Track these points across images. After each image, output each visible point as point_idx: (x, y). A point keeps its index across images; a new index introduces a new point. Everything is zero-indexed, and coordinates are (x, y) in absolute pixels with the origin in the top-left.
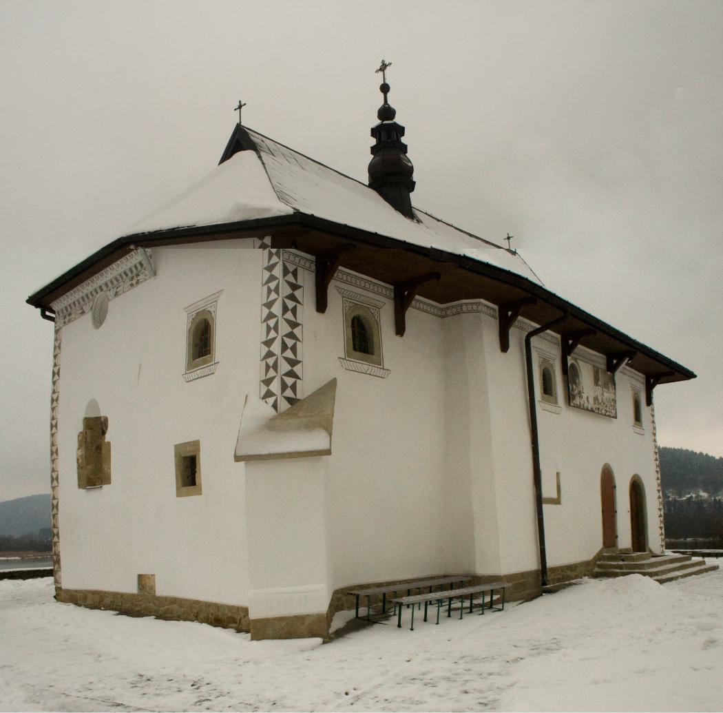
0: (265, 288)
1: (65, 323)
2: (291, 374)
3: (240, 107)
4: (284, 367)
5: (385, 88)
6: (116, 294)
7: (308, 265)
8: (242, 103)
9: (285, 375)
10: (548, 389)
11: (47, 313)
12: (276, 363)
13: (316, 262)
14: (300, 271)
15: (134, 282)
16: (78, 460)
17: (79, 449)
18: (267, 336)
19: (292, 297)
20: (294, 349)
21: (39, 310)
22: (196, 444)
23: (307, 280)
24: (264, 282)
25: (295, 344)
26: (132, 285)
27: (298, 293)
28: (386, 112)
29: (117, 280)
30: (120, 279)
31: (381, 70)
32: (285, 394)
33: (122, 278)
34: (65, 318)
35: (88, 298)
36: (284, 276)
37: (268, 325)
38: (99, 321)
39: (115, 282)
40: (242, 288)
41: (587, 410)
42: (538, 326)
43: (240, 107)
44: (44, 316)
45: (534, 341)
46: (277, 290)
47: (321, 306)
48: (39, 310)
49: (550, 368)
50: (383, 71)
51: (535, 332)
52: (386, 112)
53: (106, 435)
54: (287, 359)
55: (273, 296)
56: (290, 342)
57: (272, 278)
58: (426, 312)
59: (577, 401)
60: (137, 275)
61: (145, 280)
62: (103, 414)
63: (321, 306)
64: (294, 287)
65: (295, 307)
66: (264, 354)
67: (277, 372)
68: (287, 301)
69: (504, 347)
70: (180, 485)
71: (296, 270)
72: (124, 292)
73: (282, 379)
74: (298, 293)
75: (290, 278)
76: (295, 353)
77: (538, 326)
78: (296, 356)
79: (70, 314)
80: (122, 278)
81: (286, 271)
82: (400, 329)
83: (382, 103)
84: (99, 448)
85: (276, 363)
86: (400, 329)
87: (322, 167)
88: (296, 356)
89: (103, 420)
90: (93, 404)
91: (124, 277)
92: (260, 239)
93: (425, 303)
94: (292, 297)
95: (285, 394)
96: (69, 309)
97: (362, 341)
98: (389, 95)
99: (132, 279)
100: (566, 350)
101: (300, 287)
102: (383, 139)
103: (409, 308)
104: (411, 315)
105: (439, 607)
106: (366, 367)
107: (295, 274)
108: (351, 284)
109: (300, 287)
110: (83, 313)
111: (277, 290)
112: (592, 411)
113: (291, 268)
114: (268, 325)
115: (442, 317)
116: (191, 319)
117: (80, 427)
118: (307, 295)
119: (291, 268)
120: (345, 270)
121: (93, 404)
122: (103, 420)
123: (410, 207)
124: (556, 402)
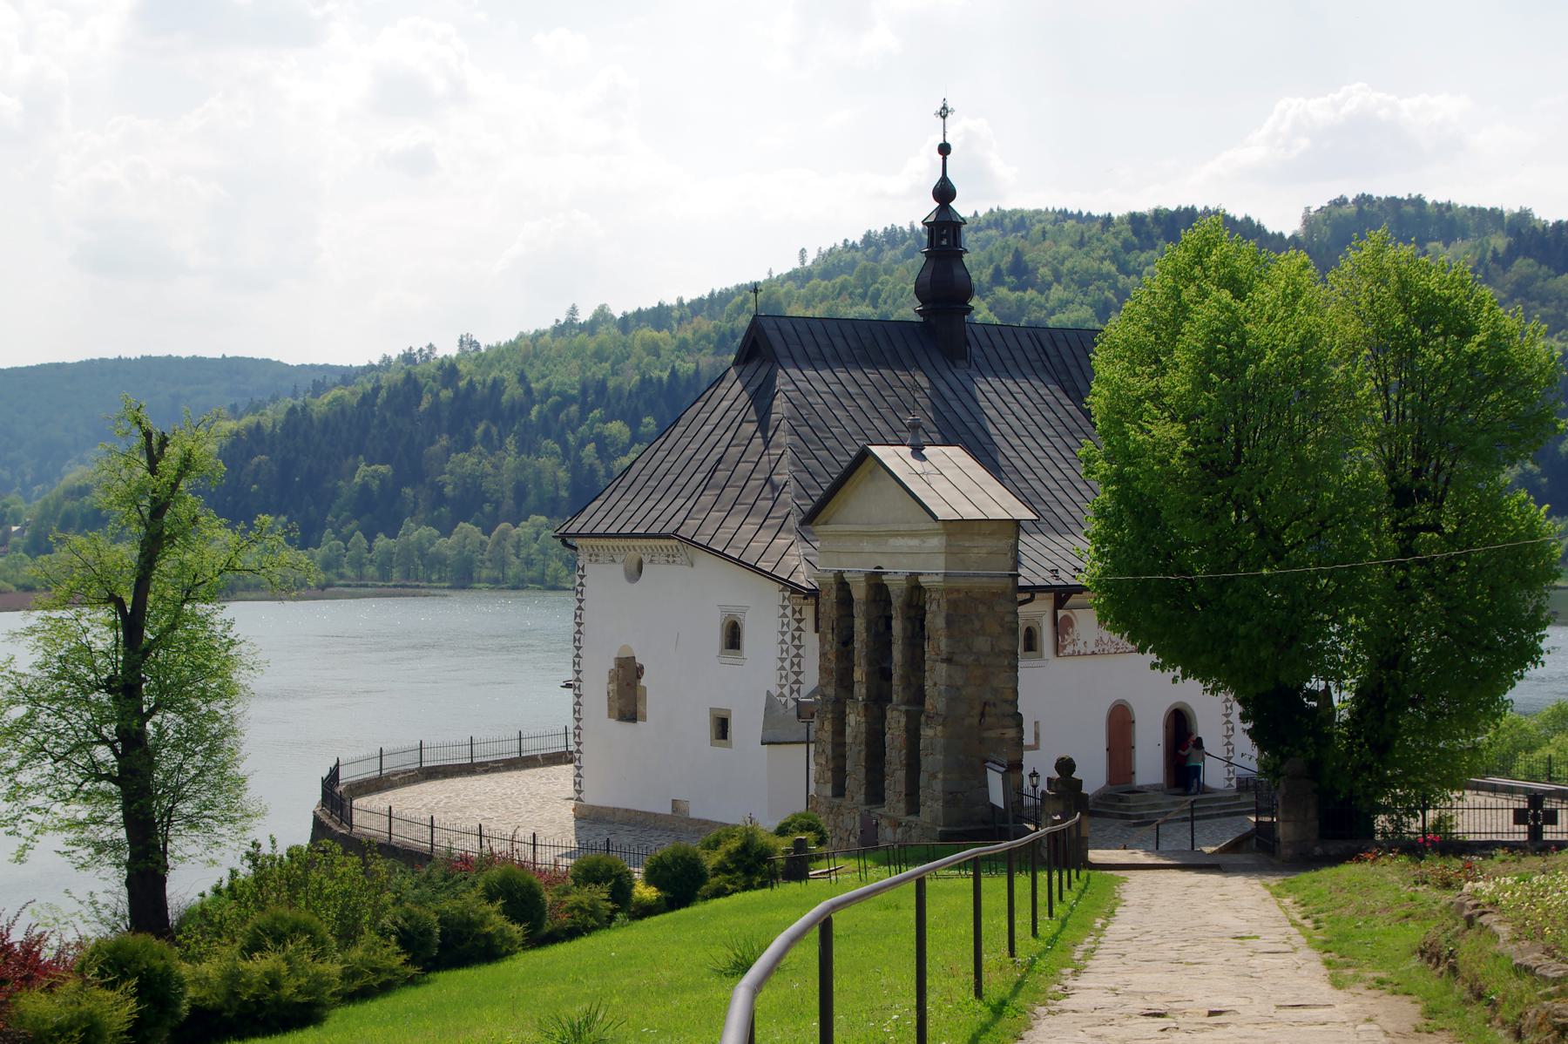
40: (1061, 613)
57: (784, 615)
59: (1069, 650)
112: (1093, 653)
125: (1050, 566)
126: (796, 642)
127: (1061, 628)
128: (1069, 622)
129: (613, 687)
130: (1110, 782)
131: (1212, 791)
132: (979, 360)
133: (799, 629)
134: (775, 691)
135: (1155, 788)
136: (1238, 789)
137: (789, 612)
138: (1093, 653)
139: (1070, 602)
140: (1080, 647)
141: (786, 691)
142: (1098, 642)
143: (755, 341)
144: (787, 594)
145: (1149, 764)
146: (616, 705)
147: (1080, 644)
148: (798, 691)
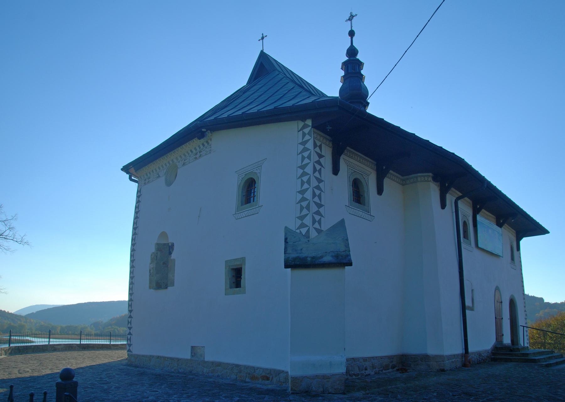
0: (300, 156)
1: (145, 183)
2: (318, 213)
3: (263, 38)
5: (352, 34)
6: (184, 164)
7: (328, 143)
8: (264, 35)
9: (314, 213)
10: (466, 236)
11: (133, 178)
12: (308, 205)
14: (323, 146)
15: (198, 156)
16: (150, 271)
17: (151, 263)
18: (301, 188)
19: (319, 163)
20: (320, 197)
21: (128, 175)
22: (243, 259)
23: (327, 152)
24: (299, 152)
25: (320, 193)
26: (196, 158)
27: (322, 160)
28: (352, 52)
29: (185, 155)
30: (187, 155)
31: (349, 19)
32: (315, 226)
33: (189, 154)
34: (145, 180)
35: (163, 167)
36: (314, 148)
37: (302, 180)
38: (169, 183)
39: (183, 157)
42: (460, 194)
43: (263, 38)
44: (131, 179)
45: (460, 203)
46: (309, 157)
47: (336, 171)
48: (128, 175)
49: (467, 221)
50: (351, 20)
51: (459, 198)
52: (352, 52)
53: (172, 255)
55: (306, 161)
56: (317, 192)
57: (306, 149)
58: (394, 180)
60: (200, 152)
61: (206, 154)
62: (170, 241)
63: (336, 171)
64: (320, 156)
65: (321, 169)
66: (298, 199)
67: (309, 211)
68: (316, 164)
69: (443, 206)
70: (228, 286)
72: (189, 163)
73: (313, 216)
74: (322, 160)
75: (317, 149)
77: (460, 194)
78: (321, 201)
79: (149, 178)
80: (189, 154)
81: (315, 145)
82: (380, 191)
83: (350, 45)
84: (166, 264)
85: (308, 205)
86: (380, 191)
87: (273, 101)
88: (321, 201)
89: (170, 245)
90: (164, 235)
91: (190, 153)
92: (302, 121)
94: (319, 163)
95: (315, 226)
96: (149, 175)
97: (358, 195)
98: (354, 38)
99: (196, 154)
100: (476, 212)
101: (324, 156)
102: (349, 71)
104: (387, 182)
107: (320, 147)
109: (324, 156)
110: (159, 177)
111: (309, 157)
113: (318, 143)
114: (302, 180)
116: (241, 178)
117: (153, 249)
118: (327, 161)
119: (318, 143)
121: (164, 235)
122: (170, 245)
124: (470, 244)
134: (292, 227)
137: (310, 145)
141: (308, 221)
143: (262, 64)
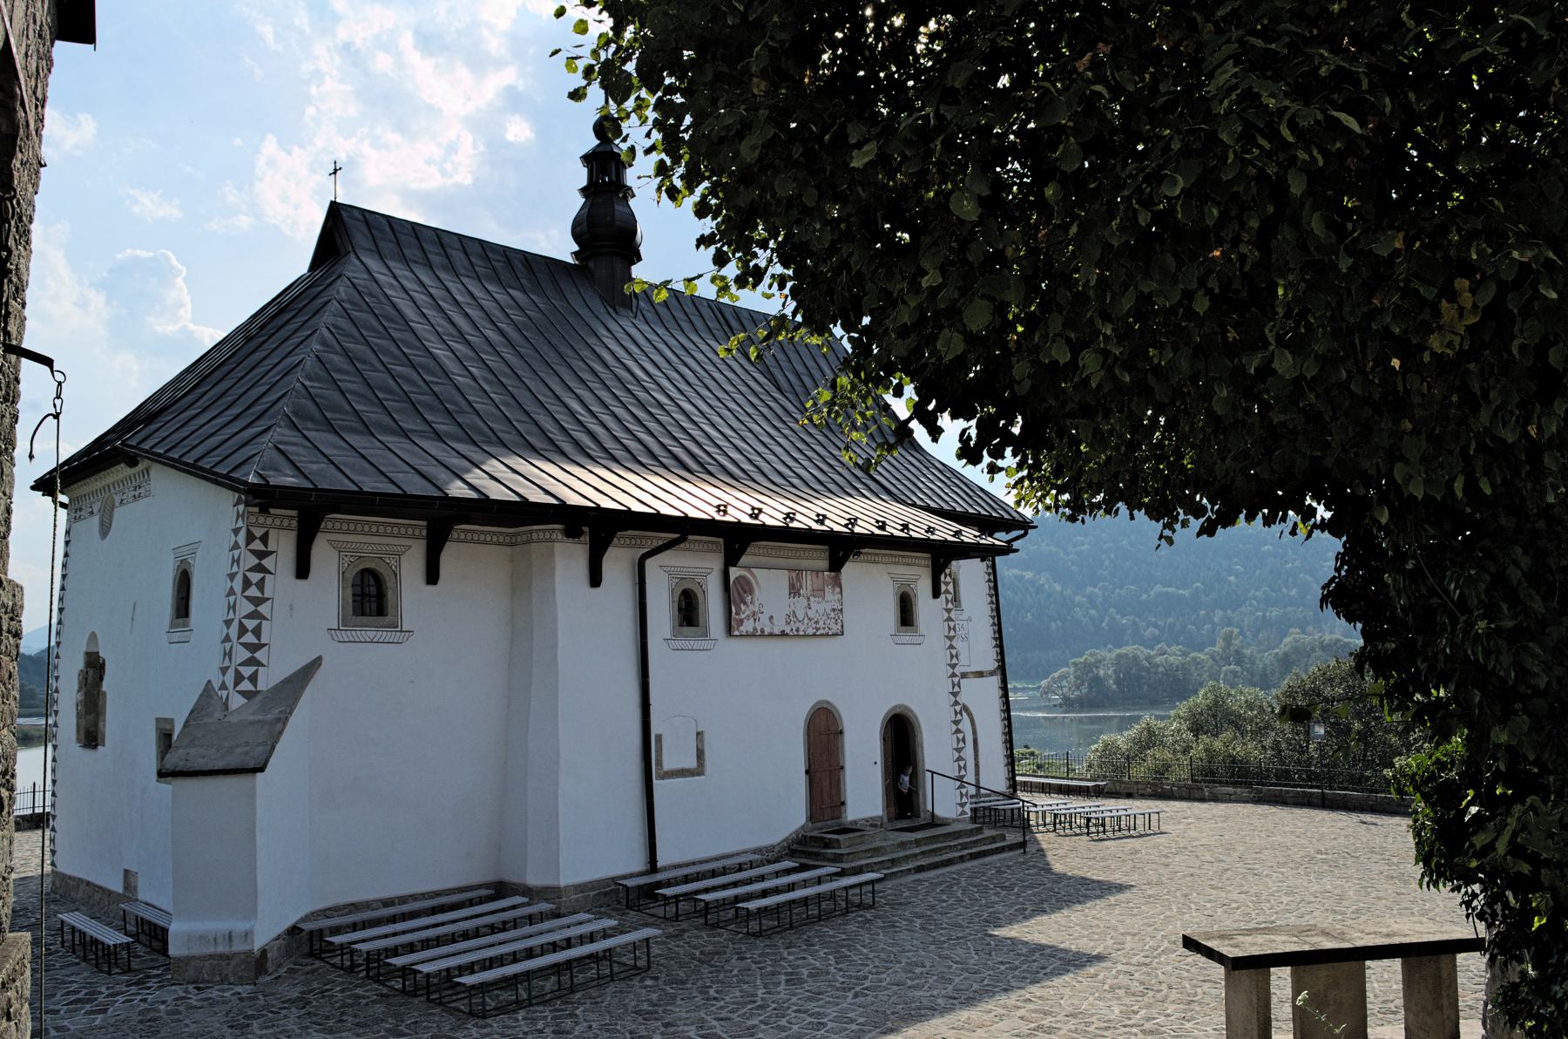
4: (242, 654)
13: (428, 528)
32: (244, 640)
40: (734, 573)
41: (771, 635)
47: (302, 571)
54: (245, 645)
56: (251, 624)
59: (748, 626)
63: (302, 571)
71: (267, 534)
76: (265, 543)
82: (432, 577)
86: (432, 577)
93: (482, 532)
97: (370, 598)
103: (319, 535)
105: (653, 866)
106: (371, 634)
108: (354, 532)
112: (783, 634)
113: (258, 532)
115: (512, 545)
119: (258, 532)
120: (278, 511)
123: (946, 564)
125: (717, 502)
126: (253, 591)
127: (733, 594)
128: (746, 587)
129: (80, 697)
130: (812, 817)
131: (943, 823)
132: (647, 314)
133: (259, 568)
135: (873, 823)
136: (974, 819)
138: (783, 634)
139: (744, 560)
140: (764, 624)
141: (230, 678)
142: (791, 617)
144: (241, 507)
145: (864, 794)
146: (83, 723)
147: (764, 618)
148: (253, 679)
